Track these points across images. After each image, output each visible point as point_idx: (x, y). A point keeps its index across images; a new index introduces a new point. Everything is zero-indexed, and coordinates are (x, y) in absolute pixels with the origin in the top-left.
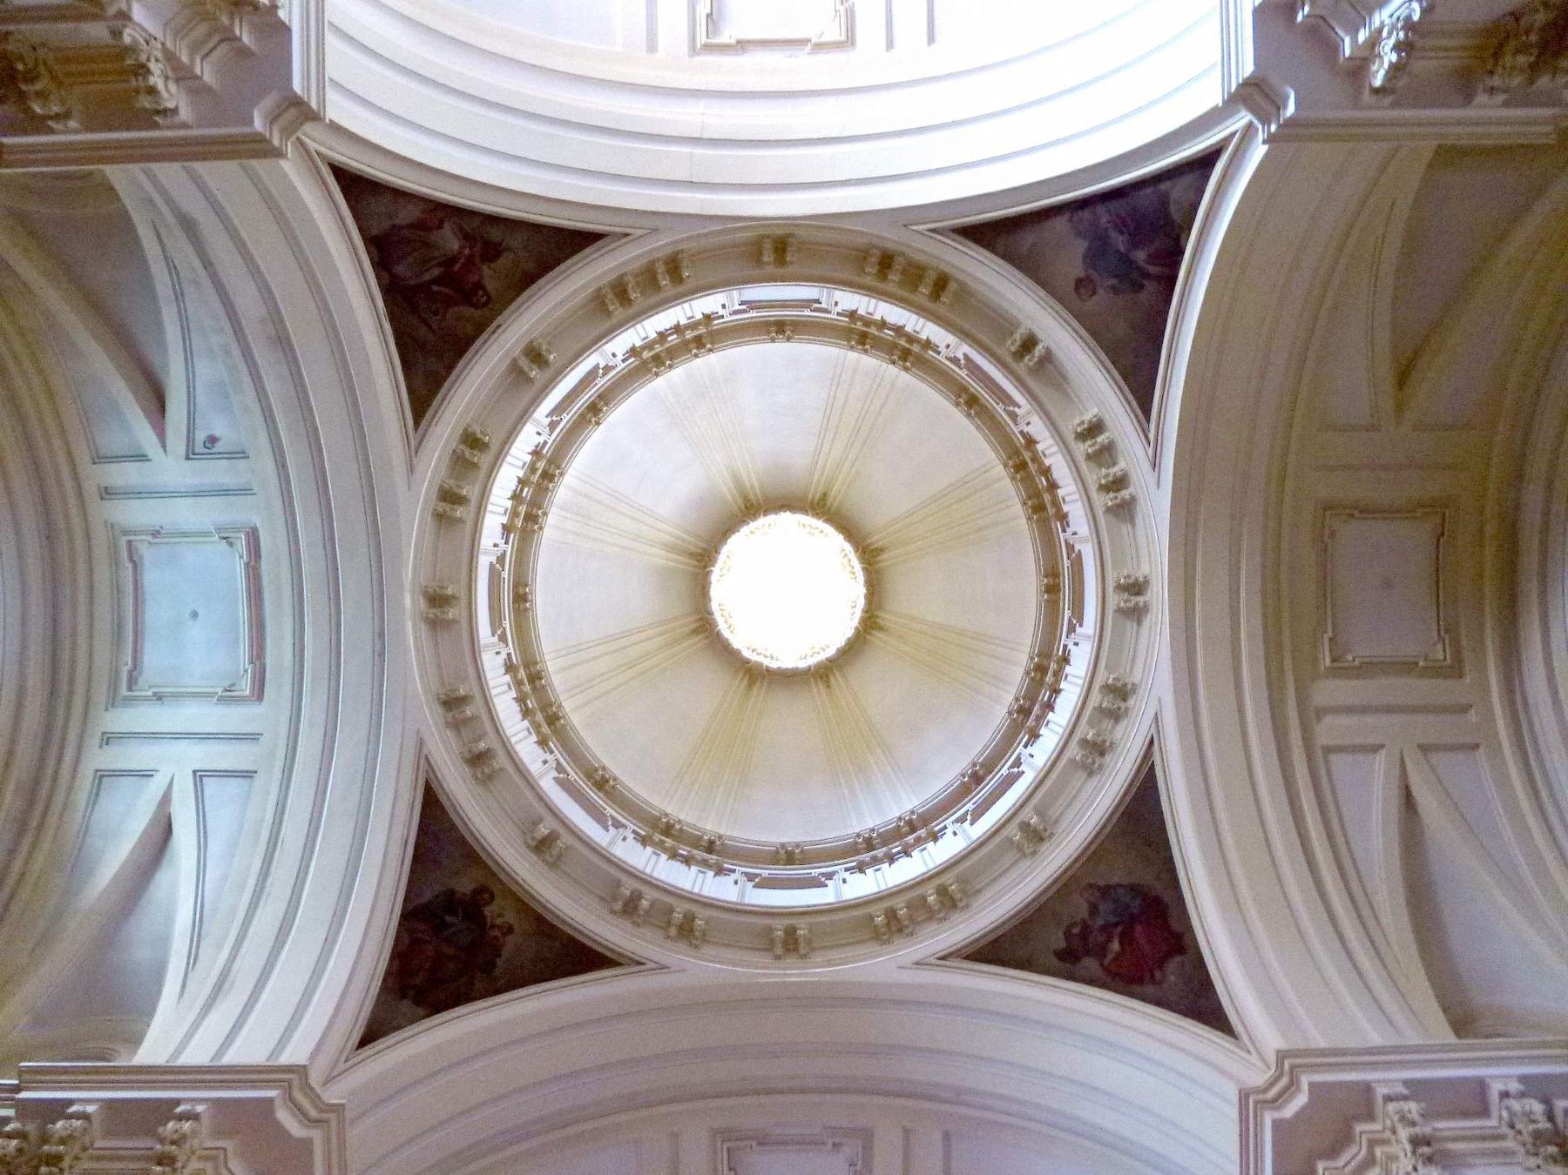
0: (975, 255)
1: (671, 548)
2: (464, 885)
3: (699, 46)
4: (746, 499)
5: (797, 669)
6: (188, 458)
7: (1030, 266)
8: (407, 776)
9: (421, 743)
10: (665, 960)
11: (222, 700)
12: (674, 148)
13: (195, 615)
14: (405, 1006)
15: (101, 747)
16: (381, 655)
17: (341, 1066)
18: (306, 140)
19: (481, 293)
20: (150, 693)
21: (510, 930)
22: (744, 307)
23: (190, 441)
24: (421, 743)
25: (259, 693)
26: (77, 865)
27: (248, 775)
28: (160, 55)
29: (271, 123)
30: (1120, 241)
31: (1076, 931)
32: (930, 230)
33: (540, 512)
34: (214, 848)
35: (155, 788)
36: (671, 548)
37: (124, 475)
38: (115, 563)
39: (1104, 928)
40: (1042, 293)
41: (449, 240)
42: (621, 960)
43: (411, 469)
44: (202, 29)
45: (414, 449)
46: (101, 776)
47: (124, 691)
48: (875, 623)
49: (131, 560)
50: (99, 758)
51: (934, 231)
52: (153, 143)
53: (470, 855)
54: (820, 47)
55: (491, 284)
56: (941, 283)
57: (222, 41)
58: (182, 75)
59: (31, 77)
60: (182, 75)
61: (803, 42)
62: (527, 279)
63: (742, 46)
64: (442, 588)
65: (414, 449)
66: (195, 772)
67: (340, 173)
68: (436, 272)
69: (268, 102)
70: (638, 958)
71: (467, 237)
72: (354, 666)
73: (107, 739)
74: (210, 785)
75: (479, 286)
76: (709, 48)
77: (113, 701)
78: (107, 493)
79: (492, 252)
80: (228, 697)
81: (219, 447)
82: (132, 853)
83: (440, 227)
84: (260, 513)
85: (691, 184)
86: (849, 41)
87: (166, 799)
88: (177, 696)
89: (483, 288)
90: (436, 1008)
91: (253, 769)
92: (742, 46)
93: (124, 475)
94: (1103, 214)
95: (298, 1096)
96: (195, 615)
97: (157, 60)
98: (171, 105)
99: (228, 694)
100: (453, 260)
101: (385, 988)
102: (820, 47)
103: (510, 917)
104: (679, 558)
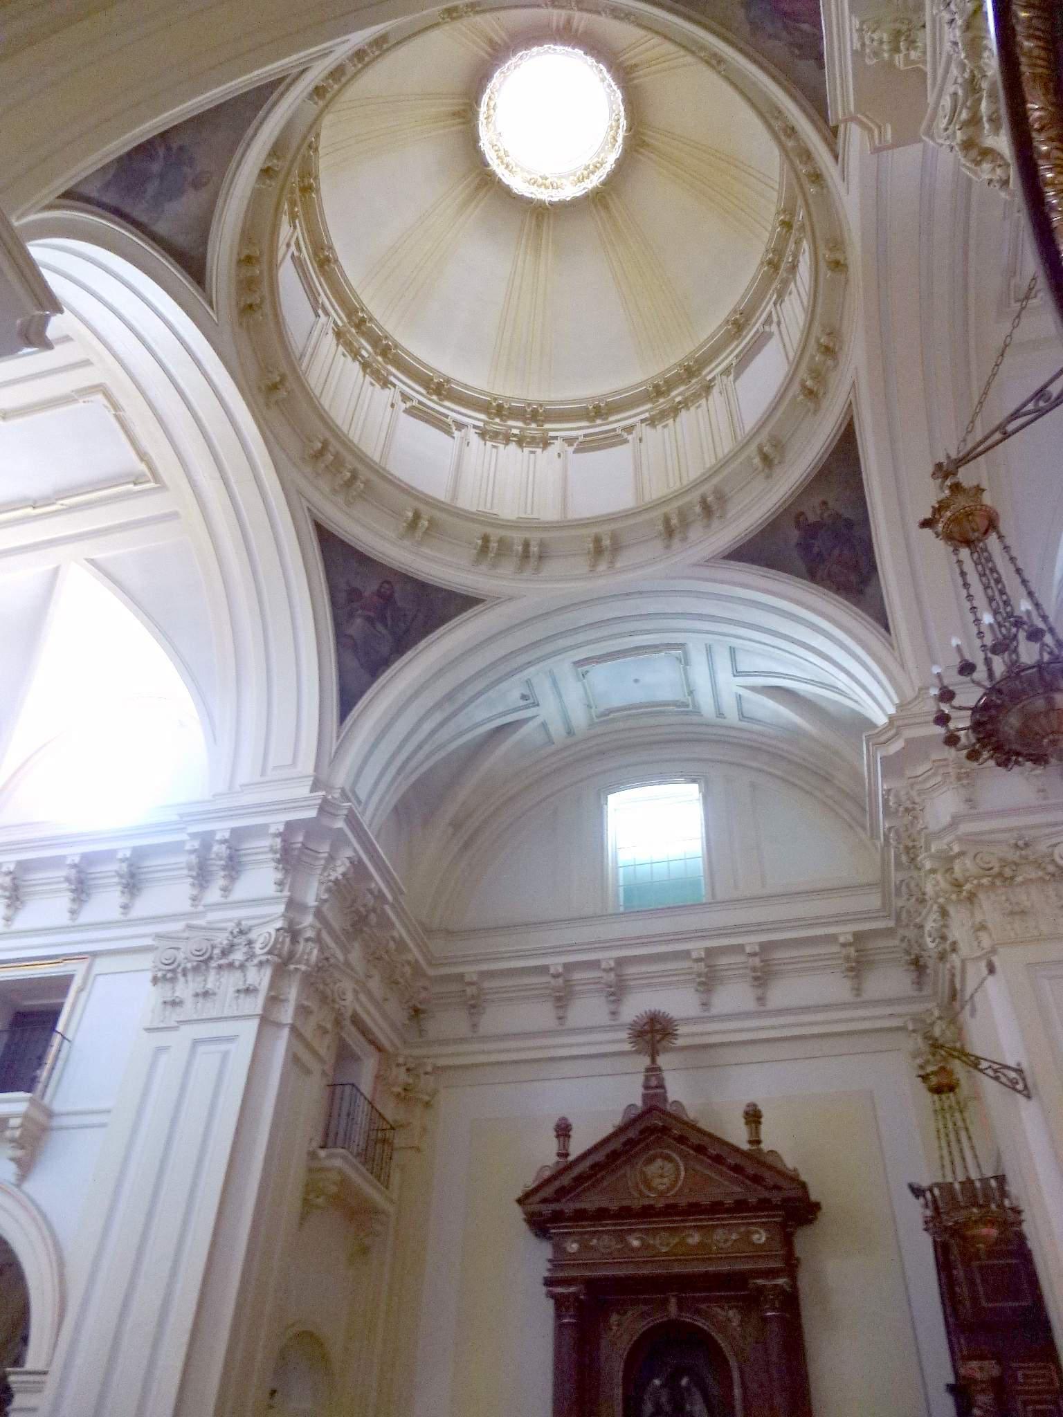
0: (215, 268)
1: (537, 250)
2: (794, 535)
3: (158, 485)
4: (478, 188)
5: (623, 100)
6: (538, 705)
7: (203, 227)
8: (720, 574)
9: (695, 565)
10: (846, 387)
11: (687, 663)
12: (239, 498)
13: (636, 681)
14: (869, 590)
15: (725, 718)
16: (640, 593)
17: (897, 654)
18: (333, 751)
19: (383, 590)
20: (689, 697)
21: (825, 503)
22: (320, 311)
23: (527, 707)
24: (695, 565)
25: (681, 646)
26: (794, 734)
27: (733, 651)
28: (326, 874)
29: (337, 815)
30: (152, 188)
31: (797, 52)
32: (212, 308)
33: (529, 410)
34: (781, 670)
35: (746, 694)
36: (537, 250)
37: (557, 729)
38: (613, 720)
39: (790, 33)
40: (220, 203)
41: (357, 626)
42: (848, 418)
43: (511, 599)
44: (304, 858)
45: (498, 600)
46: (742, 716)
47: (690, 708)
48: (564, 28)
49: (608, 715)
50: (732, 716)
51: (211, 305)
52: (371, 858)
53: (772, 528)
54: (115, 406)
55: (373, 587)
56: (247, 261)
57: (307, 848)
58: (331, 858)
59: (357, 912)
60: (331, 858)
61: (118, 418)
62: (363, 560)
63: (142, 456)
64: (589, 553)
65: (498, 600)
66: (734, 676)
67: (343, 716)
68: (380, 627)
69: (326, 821)
70: (846, 406)
71: (351, 615)
72: (652, 606)
73: (720, 714)
74: (742, 667)
75: (379, 594)
76: (156, 477)
77: (697, 712)
78: (570, 732)
79: (354, 595)
80: (685, 661)
81: (527, 692)
82: (785, 707)
83: (351, 636)
84: (563, 667)
85: (257, 478)
86: (101, 389)
87: (753, 689)
88: (688, 685)
89: (379, 591)
90: (873, 568)
91: (728, 650)
92: (142, 456)
93: (557, 729)
94: (138, 213)
95: (883, 739)
96: (636, 681)
97: (329, 875)
98: (348, 864)
99: (683, 660)
100: (369, 619)
101: (857, 604)
102: (115, 406)
103: (816, 501)
104: (544, 229)
